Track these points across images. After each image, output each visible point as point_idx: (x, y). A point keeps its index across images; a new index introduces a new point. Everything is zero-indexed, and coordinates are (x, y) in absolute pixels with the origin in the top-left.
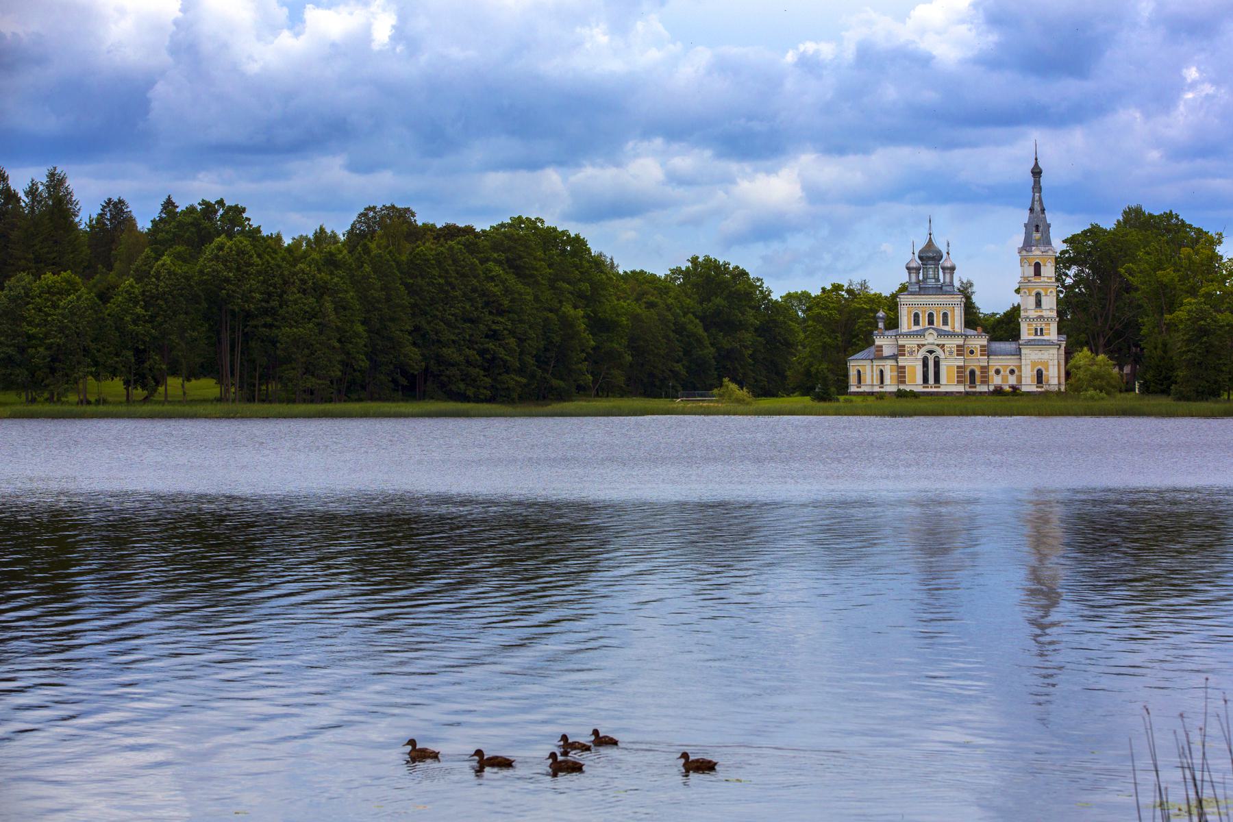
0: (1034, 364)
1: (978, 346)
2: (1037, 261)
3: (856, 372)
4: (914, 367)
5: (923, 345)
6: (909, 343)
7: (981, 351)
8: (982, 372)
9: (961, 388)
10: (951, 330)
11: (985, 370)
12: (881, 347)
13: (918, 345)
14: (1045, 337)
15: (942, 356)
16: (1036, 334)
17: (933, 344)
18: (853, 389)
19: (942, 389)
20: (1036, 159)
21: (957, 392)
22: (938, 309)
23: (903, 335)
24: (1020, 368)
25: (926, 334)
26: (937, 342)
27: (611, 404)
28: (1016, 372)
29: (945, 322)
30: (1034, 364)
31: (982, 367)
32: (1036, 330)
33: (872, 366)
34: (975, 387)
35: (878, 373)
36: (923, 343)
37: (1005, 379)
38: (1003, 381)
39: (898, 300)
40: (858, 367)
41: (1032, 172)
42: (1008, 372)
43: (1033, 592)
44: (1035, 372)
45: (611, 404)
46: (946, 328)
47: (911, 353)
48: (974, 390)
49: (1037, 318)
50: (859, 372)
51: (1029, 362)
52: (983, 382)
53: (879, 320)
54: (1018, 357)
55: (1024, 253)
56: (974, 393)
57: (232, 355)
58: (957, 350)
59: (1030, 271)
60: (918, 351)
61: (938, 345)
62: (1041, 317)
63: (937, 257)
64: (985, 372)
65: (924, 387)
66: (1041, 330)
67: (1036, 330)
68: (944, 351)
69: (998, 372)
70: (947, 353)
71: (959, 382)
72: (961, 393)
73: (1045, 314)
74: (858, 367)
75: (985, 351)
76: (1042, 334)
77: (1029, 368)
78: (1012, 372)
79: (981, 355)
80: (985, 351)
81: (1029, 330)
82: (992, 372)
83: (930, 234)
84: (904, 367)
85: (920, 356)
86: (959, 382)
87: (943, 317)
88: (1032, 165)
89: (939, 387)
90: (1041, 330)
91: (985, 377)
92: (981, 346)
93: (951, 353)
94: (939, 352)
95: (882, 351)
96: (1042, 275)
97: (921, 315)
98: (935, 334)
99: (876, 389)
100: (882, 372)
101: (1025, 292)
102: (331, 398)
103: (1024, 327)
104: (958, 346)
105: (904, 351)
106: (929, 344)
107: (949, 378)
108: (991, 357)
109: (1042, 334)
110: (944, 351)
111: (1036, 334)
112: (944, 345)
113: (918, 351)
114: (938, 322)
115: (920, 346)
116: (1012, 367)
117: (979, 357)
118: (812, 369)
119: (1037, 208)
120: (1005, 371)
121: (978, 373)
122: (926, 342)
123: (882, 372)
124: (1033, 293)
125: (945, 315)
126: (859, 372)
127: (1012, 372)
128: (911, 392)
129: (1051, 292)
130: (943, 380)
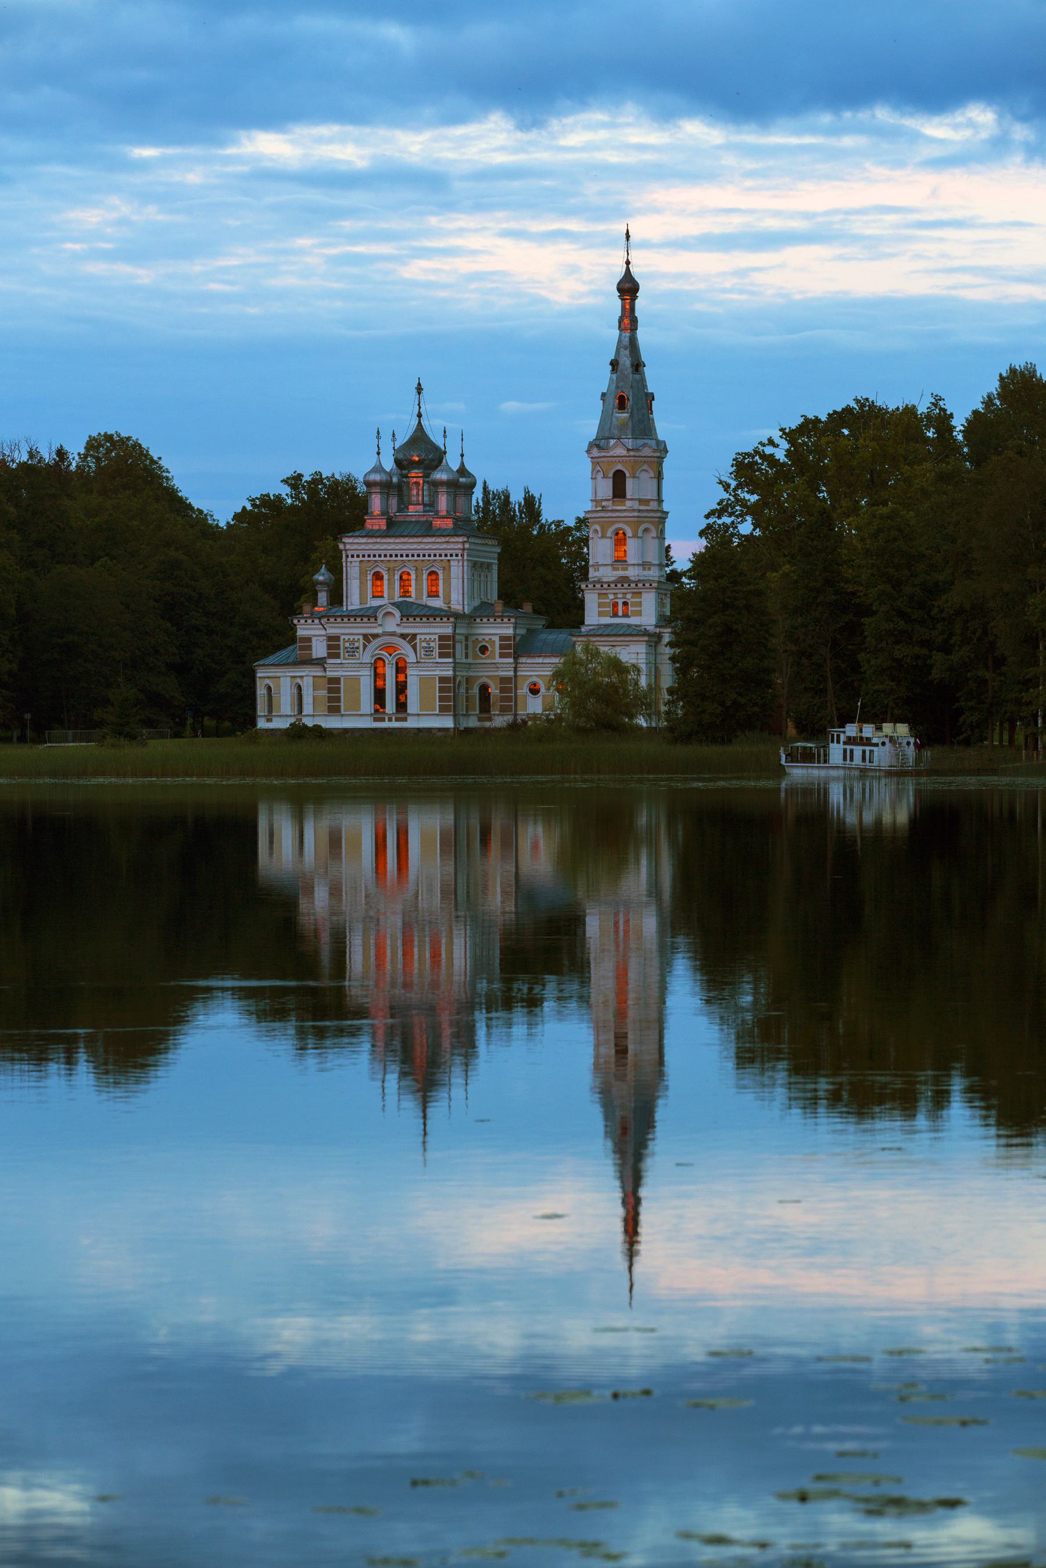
1: (496, 639)
2: (619, 467)
4: (357, 679)
5: (375, 636)
6: (349, 632)
7: (501, 647)
9: (448, 722)
10: (444, 607)
11: (508, 684)
12: (309, 639)
13: (365, 636)
14: (633, 620)
15: (411, 658)
17: (393, 634)
18: (262, 724)
19: (411, 723)
21: (440, 730)
22: (392, 565)
23: (349, 616)
25: (380, 615)
31: (504, 680)
32: (615, 605)
34: (490, 719)
39: (341, 546)
40: (267, 681)
41: (619, 290)
43: (476, 1065)
46: (437, 603)
47: (352, 651)
48: (487, 724)
49: (616, 583)
52: (504, 710)
53: (318, 588)
55: (595, 452)
58: (441, 647)
59: (606, 488)
60: (365, 646)
61: (403, 636)
62: (624, 580)
63: (435, 457)
65: (375, 720)
68: (414, 647)
69: (534, 691)
72: (447, 730)
73: (632, 573)
75: (508, 647)
79: (502, 656)
80: (508, 647)
81: (600, 605)
82: (524, 690)
84: (337, 680)
85: (367, 658)
86: (443, 709)
89: (405, 719)
91: (509, 699)
92: (503, 638)
93: (429, 651)
94: (405, 649)
95: (310, 648)
97: (386, 577)
98: (397, 614)
101: (596, 531)
103: (591, 601)
104: (442, 638)
106: (385, 634)
107: (424, 704)
108: (522, 660)
109: (626, 615)
111: (615, 615)
112: (414, 636)
113: (365, 646)
114: (419, 590)
117: (498, 660)
118: (718, 711)
119: (626, 361)
121: (494, 690)
126: (269, 689)
128: (317, 728)
129: (646, 530)
130: (413, 707)
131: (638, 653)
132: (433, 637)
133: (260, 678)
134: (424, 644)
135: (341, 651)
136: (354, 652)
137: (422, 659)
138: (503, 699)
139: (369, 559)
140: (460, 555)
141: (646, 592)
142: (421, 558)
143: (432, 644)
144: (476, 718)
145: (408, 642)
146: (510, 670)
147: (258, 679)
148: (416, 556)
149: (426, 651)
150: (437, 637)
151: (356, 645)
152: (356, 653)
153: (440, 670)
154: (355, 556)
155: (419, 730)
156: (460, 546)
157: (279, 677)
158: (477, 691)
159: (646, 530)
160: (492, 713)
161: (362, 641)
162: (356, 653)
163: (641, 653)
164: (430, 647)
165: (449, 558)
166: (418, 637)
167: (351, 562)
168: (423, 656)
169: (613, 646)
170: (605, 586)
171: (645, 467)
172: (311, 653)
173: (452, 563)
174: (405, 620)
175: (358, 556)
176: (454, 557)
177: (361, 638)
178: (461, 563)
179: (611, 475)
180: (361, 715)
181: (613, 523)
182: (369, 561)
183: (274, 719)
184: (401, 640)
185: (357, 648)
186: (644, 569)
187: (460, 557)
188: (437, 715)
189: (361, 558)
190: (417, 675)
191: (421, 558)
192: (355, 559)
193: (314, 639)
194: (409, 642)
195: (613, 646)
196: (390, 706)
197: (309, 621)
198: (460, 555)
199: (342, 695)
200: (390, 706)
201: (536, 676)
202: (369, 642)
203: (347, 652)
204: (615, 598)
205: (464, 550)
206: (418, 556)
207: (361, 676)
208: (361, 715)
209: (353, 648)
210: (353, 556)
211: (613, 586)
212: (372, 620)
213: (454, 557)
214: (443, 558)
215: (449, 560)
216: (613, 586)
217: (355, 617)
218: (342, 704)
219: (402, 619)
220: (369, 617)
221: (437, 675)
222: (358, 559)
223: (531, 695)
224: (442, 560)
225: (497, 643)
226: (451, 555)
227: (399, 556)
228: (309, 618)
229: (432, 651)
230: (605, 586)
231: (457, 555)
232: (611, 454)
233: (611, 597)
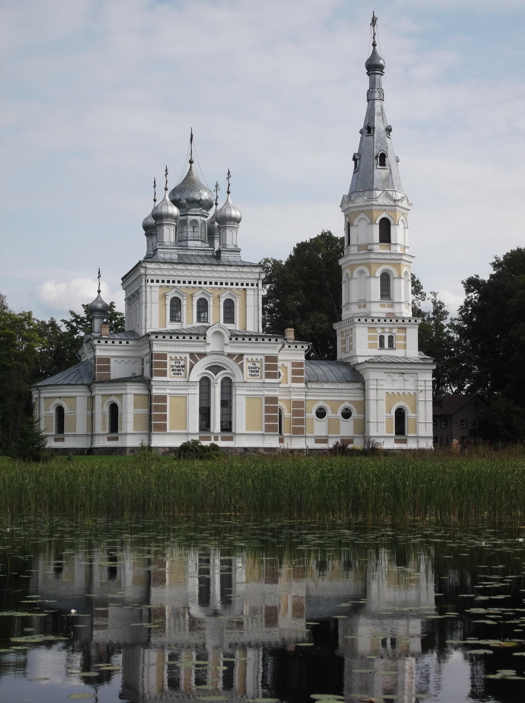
0: (391, 397)
1: (289, 365)
2: (384, 215)
3: (53, 411)
5: (203, 355)
7: (294, 372)
8: (295, 413)
13: (192, 355)
14: (398, 353)
15: (237, 379)
16: (382, 345)
17: (220, 353)
20: (374, 45)
21: (266, 449)
24: (363, 407)
26: (228, 350)
27: (237, 676)
28: (355, 414)
29: (229, 317)
30: (391, 397)
32: (382, 338)
33: (92, 398)
35: (107, 410)
36: (202, 350)
37: (333, 427)
38: (329, 430)
42: (339, 414)
44: (393, 414)
45: (237, 676)
48: (403, 446)
50: (60, 410)
51: (382, 395)
54: (359, 385)
56: (65, 451)
57: (305, 547)
61: (230, 356)
64: (302, 413)
65: (109, 439)
66: (391, 338)
67: (382, 338)
69: (321, 413)
70: (247, 372)
71: (269, 429)
74: (58, 401)
76: (391, 345)
77: (383, 405)
78: (347, 414)
79: (294, 380)
81: (370, 338)
83: (191, 162)
85: (196, 376)
86: (269, 429)
87: (225, 308)
88: (368, 54)
90: (391, 338)
95: (108, 368)
96: (393, 241)
99: (102, 442)
100: (114, 409)
102: (414, 457)
105: (165, 365)
106: (213, 353)
110: (241, 366)
112: (241, 356)
115: (195, 357)
116: (347, 405)
120: (334, 411)
122: (208, 349)
123: (114, 409)
124: (378, 274)
125: (229, 306)
126: (60, 410)
127: (347, 414)
131: (425, 381)
132: (259, 358)
133: (45, 398)
134: (251, 365)
135: (264, 371)
136: (180, 370)
137: (249, 378)
138: (296, 422)
139: (168, 284)
140: (255, 285)
141: (410, 328)
142: (219, 286)
143: (258, 365)
144: (106, 438)
145: (196, 363)
146: (303, 395)
147: (384, 399)
148: (213, 283)
149: (252, 372)
150: (263, 358)
151: (182, 363)
152: (181, 372)
153: (247, 390)
154: (155, 281)
155: (246, 449)
156: (257, 276)
157: (75, 397)
158: (394, 415)
159: (361, 272)
160: (65, 433)
161: (189, 359)
162: (181, 372)
163: (379, 380)
164: (256, 368)
165: (245, 287)
166: (245, 357)
167: (151, 287)
168: (249, 376)
169: (403, 373)
170: (376, 320)
171: (362, 215)
172: (109, 374)
173: (248, 292)
174: (234, 339)
175: (158, 281)
176: (250, 287)
177: (188, 356)
178: (256, 291)
179: (378, 222)
180: (75, 435)
181: (381, 264)
182: (168, 286)
183: (66, 438)
184: (228, 359)
185: (183, 366)
186: (360, 307)
187: (255, 287)
188: (263, 435)
189: (160, 283)
190: (245, 395)
191: (219, 286)
192: (155, 283)
193: (112, 361)
194: (237, 361)
195: (403, 373)
196: (216, 425)
197: (110, 342)
198: (255, 285)
199: (168, 413)
200: (216, 425)
201: (323, 400)
202: (196, 361)
203: (173, 370)
204: (382, 332)
205: (259, 279)
206: (216, 283)
207: (188, 394)
208: (75, 435)
209: (178, 367)
210: (152, 281)
211: (382, 321)
212: (201, 338)
213: (250, 287)
214: (240, 286)
215: (245, 289)
216: (382, 321)
217: (184, 335)
218: (168, 423)
219: (231, 339)
220: (198, 335)
221: (264, 395)
222: (158, 284)
223: (343, 419)
224: (238, 289)
225: (290, 369)
226: (247, 285)
227: (197, 283)
228: (109, 339)
229: (258, 372)
230: (376, 320)
231: (252, 285)
232: (355, 204)
233: (379, 331)
